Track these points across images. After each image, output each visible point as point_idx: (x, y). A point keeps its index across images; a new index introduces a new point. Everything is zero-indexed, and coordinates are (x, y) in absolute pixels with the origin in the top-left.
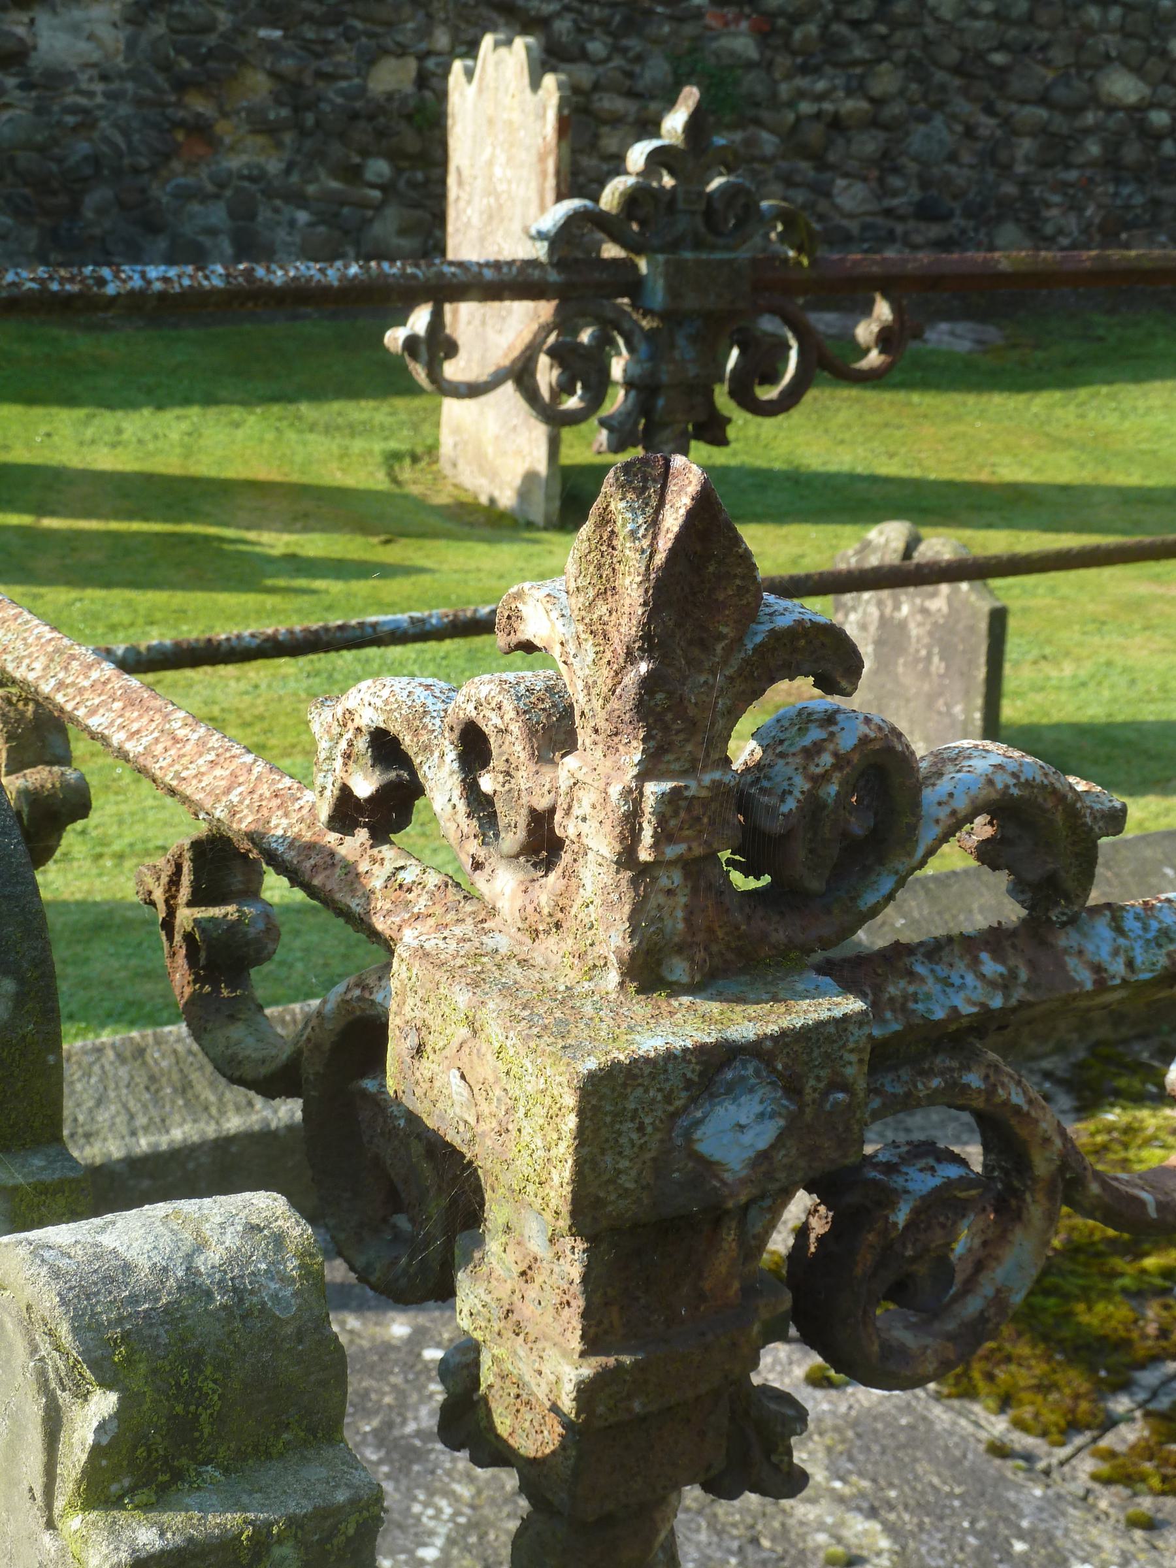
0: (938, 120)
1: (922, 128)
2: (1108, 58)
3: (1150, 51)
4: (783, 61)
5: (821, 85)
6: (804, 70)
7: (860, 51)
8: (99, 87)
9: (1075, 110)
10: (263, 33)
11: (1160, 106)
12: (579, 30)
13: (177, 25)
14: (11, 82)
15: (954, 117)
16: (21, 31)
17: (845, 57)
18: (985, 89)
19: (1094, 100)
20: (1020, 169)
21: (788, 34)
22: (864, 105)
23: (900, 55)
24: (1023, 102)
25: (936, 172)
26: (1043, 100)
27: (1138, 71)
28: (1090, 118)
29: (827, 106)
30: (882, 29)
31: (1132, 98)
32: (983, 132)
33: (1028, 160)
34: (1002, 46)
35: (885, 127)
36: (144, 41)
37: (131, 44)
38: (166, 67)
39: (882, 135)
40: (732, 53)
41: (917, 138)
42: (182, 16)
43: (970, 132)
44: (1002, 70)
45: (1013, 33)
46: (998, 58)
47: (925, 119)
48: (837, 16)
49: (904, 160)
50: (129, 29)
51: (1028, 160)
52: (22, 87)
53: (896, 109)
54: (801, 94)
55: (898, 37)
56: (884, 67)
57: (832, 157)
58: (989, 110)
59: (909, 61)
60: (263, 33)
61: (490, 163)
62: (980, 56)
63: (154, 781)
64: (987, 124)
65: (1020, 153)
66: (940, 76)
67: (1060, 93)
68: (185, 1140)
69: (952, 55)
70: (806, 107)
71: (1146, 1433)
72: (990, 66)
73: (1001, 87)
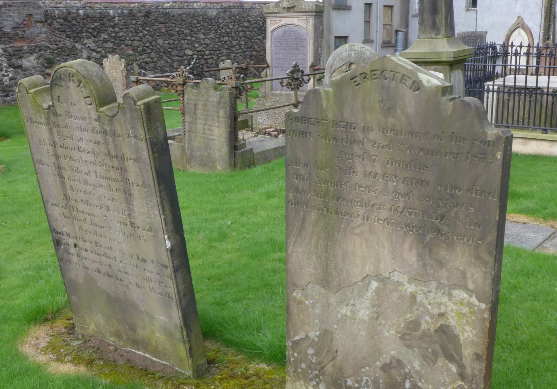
0: (162, 60)
1: (160, 62)
2: (186, 48)
3: (192, 46)
4: (137, 54)
5: (143, 57)
6: (140, 55)
7: (149, 51)
8: (33, 70)
9: (182, 57)
10: (57, 58)
11: (195, 55)
12: (106, 53)
13: (44, 58)
14: (20, 70)
15: (164, 60)
16: (20, 62)
17: (146, 52)
18: (168, 55)
19: (185, 55)
20: (175, 67)
21: (137, 50)
22: (150, 59)
23: (155, 51)
24: (174, 56)
25: (162, 69)
26: (177, 56)
27: (191, 50)
28: (185, 57)
29: (145, 60)
30: (151, 47)
31: (191, 54)
32: (169, 61)
33: (177, 65)
34: (170, 48)
35: (154, 62)
36: (40, 61)
37: (38, 63)
38: (43, 66)
39: (154, 64)
40: (129, 53)
41: (159, 64)
42: (45, 57)
43: (167, 62)
44: (170, 52)
45: (171, 46)
46: (170, 50)
47: (159, 61)
48: (144, 46)
49: (157, 67)
50: (37, 60)
51: (177, 65)
52: (22, 71)
53: (155, 59)
54: (141, 59)
55: (154, 48)
56: (152, 53)
57: (147, 68)
58: (169, 58)
59: (156, 51)
60: (57, 58)
61: (113, 72)
62: (167, 50)
63: (12, 182)
64: (169, 60)
65: (175, 64)
66: (161, 54)
67: (179, 54)
68: (225, 138)
69: (162, 50)
70: (141, 61)
71: (49, 370)
72: (168, 51)
73: (170, 54)
